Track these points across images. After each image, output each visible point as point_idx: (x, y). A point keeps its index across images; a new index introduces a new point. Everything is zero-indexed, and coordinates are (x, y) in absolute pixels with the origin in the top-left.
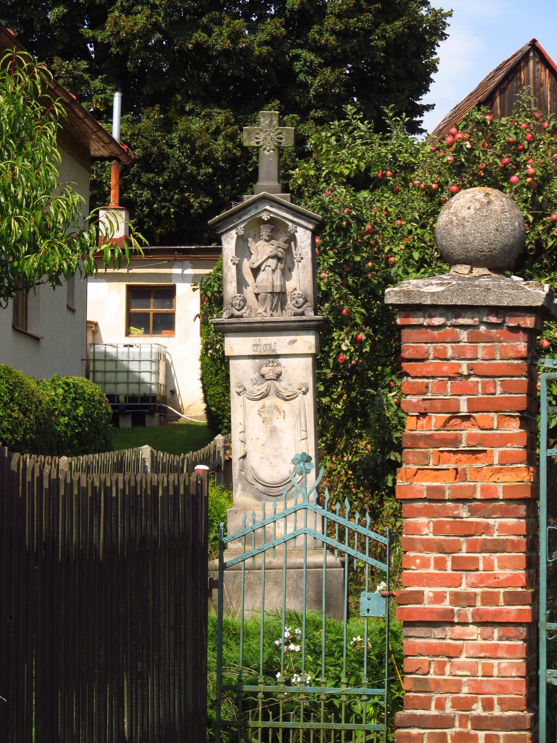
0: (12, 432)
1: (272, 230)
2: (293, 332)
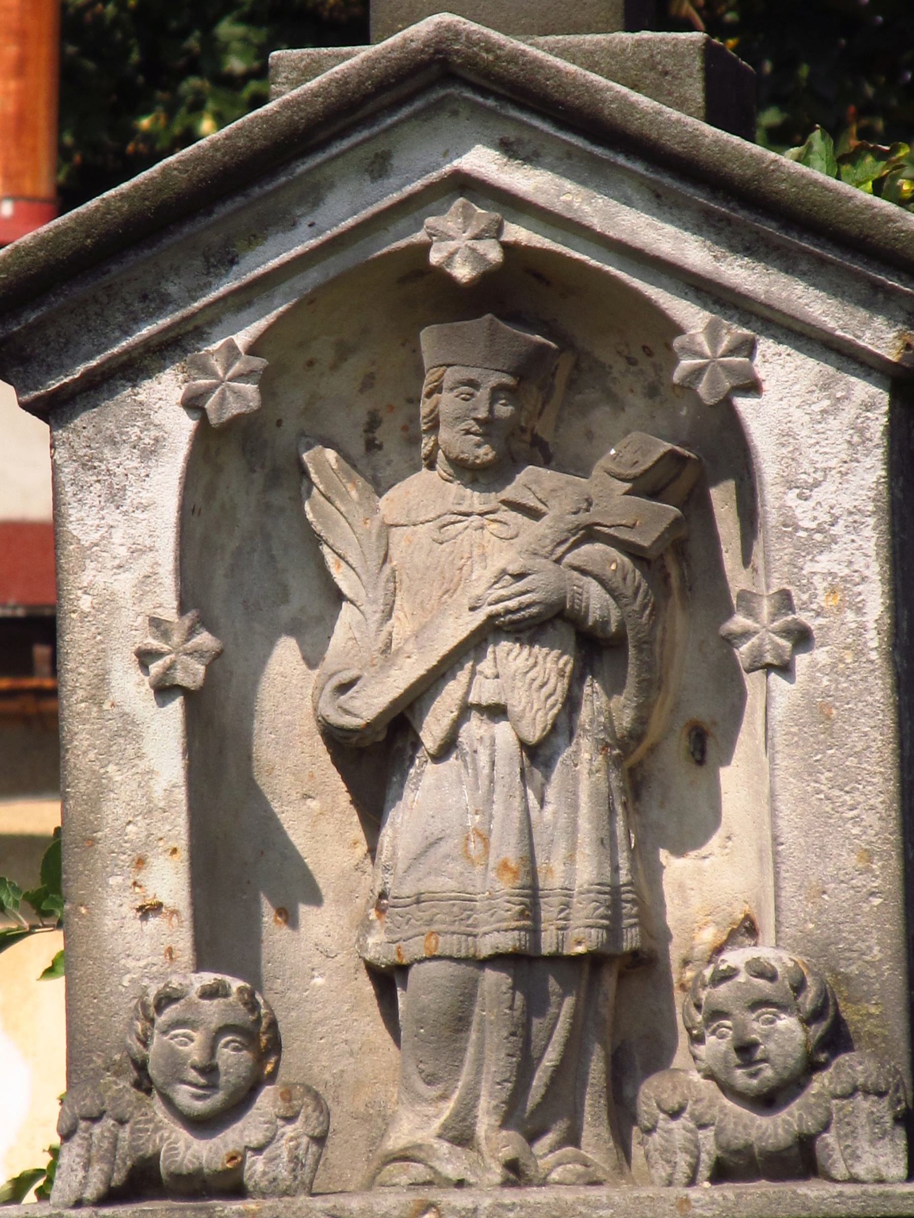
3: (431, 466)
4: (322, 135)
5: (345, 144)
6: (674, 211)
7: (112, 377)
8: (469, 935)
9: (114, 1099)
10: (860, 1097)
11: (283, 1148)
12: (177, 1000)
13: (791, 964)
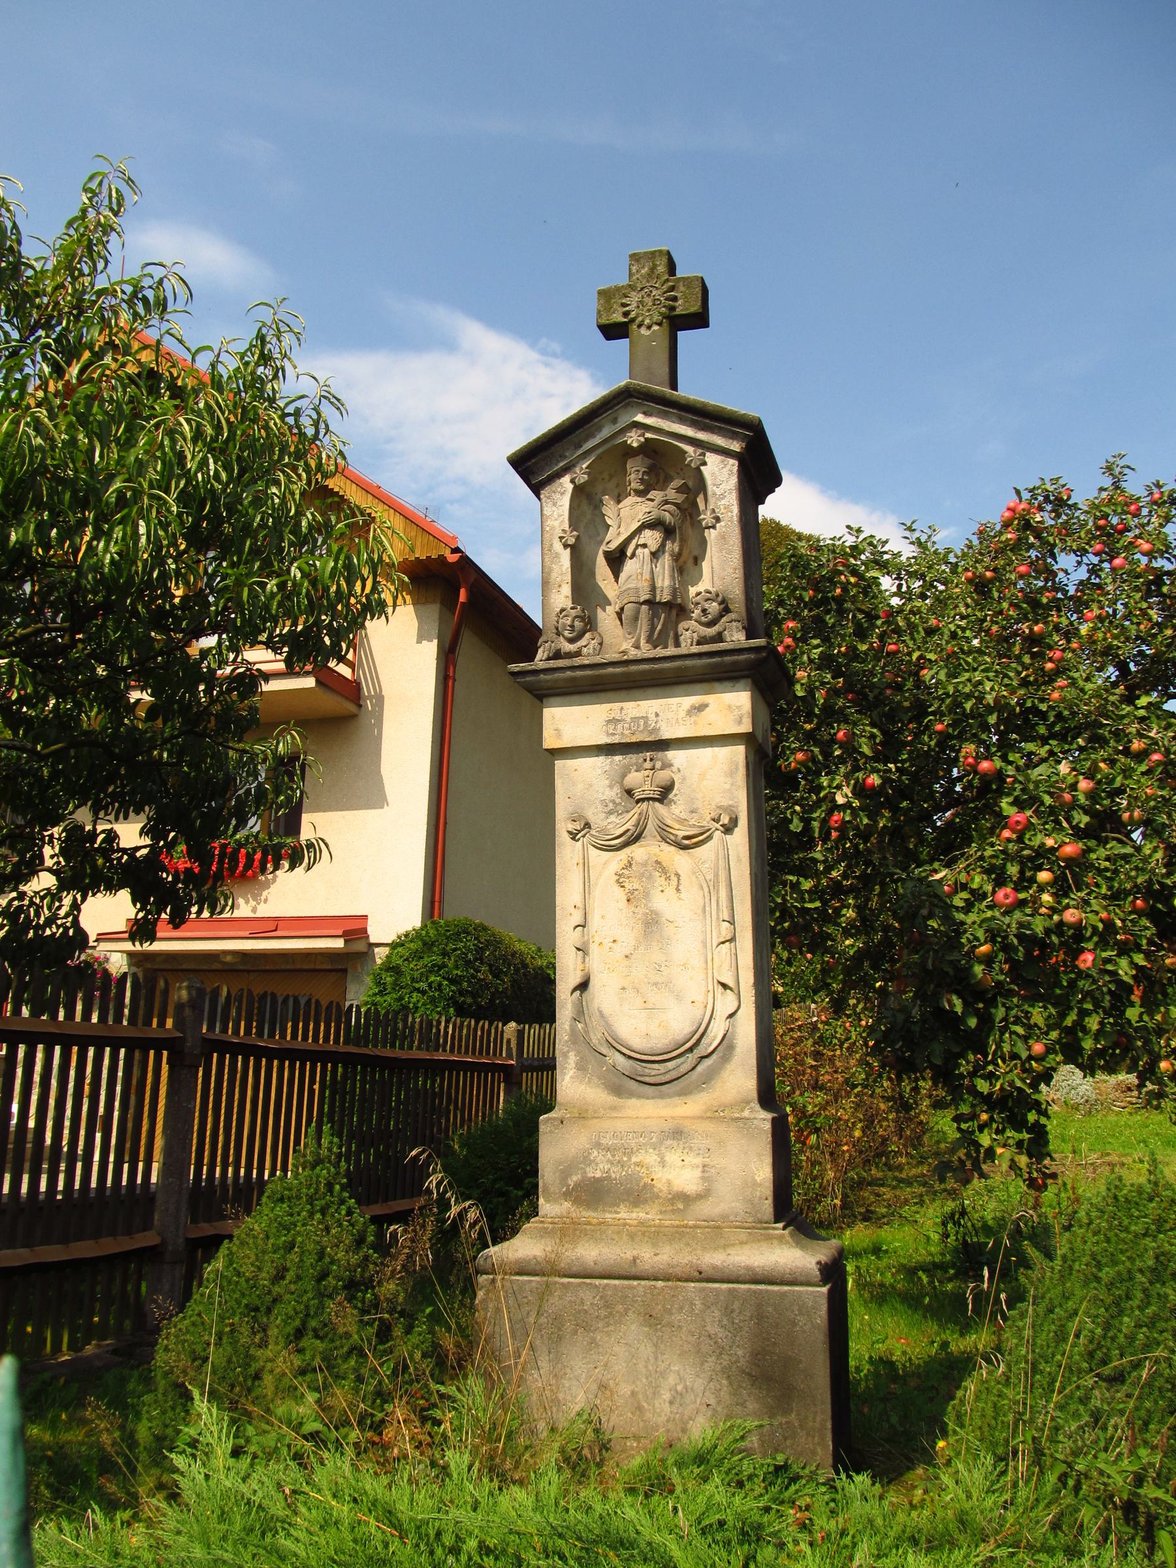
0: (474, 995)
1: (651, 470)
2: (698, 687)
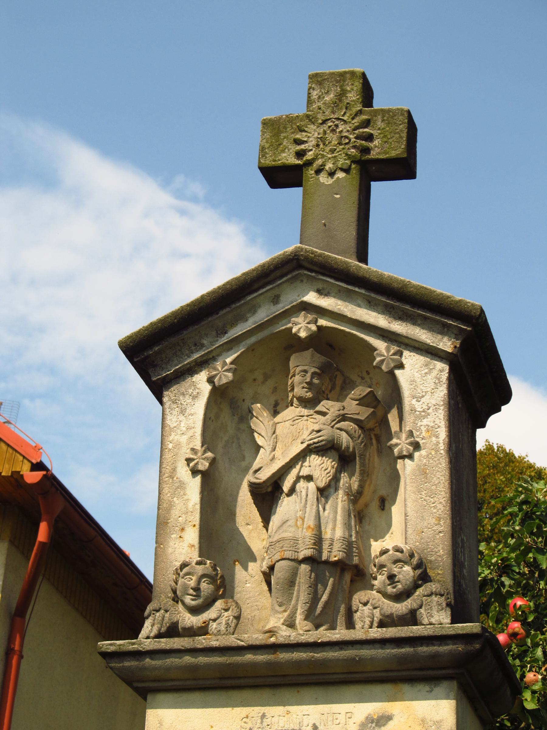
1: (324, 371)
2: (377, 689)
3: (292, 405)
4: (256, 286)
5: (264, 290)
6: (375, 307)
7: (184, 374)
8: (295, 552)
9: (165, 604)
10: (434, 596)
11: (223, 620)
12: (188, 565)
13: (409, 548)
